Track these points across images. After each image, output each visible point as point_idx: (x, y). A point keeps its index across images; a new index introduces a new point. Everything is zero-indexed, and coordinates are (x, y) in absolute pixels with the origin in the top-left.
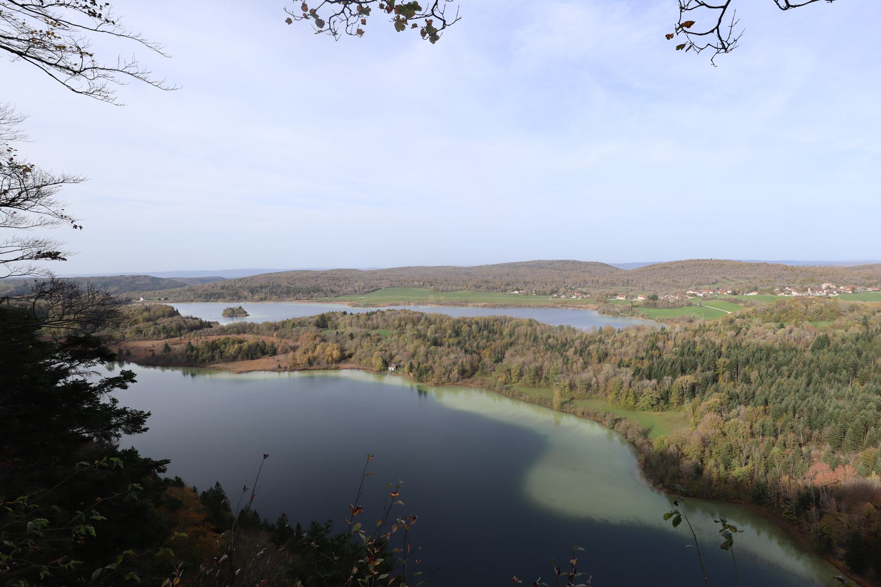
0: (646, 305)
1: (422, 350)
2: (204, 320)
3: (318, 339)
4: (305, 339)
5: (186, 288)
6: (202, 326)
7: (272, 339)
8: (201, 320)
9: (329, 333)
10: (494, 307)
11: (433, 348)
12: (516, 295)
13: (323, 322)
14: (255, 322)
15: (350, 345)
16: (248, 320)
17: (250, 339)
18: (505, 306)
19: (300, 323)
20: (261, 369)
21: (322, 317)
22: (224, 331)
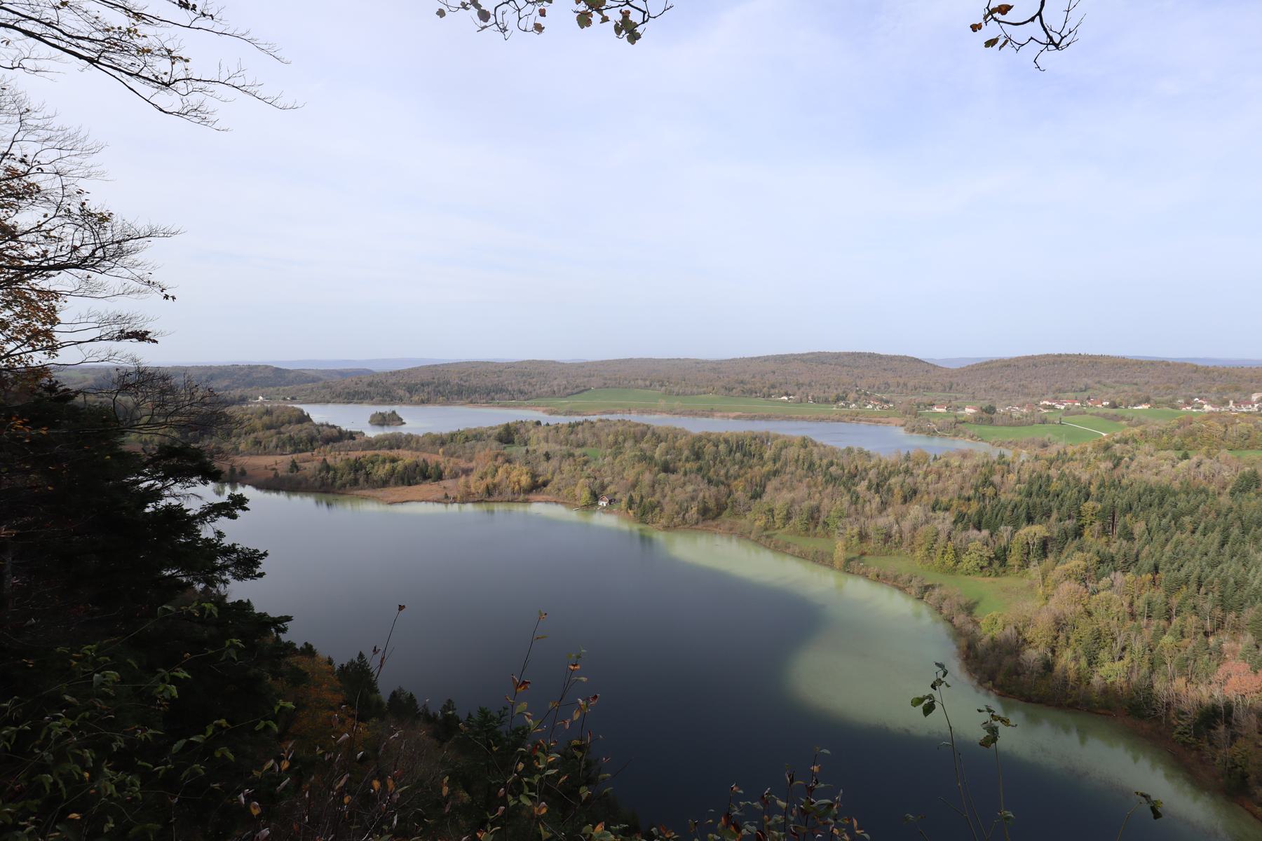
0: (978, 420)
2: (344, 428)
4: (482, 459)
5: (321, 384)
6: (338, 437)
7: (435, 458)
8: (340, 429)
9: (516, 451)
11: (662, 475)
12: (784, 401)
13: (508, 436)
14: (413, 433)
15: (545, 468)
16: (404, 430)
17: (407, 457)
18: (767, 418)
19: (475, 436)
20: (421, 498)
22: (371, 444)
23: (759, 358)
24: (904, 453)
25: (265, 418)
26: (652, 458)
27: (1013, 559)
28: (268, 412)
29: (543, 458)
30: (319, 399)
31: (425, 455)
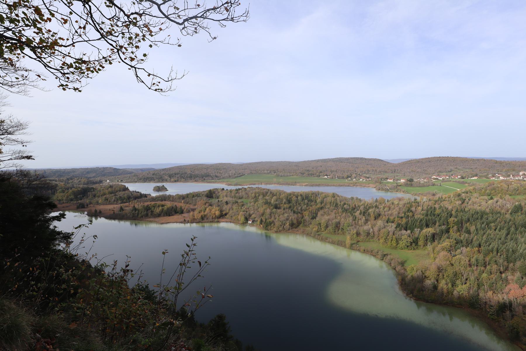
0: (406, 185)
1: (268, 211)
2: (142, 193)
5: (133, 174)
6: (140, 196)
7: (181, 204)
9: (214, 201)
10: (312, 186)
11: (274, 210)
12: (325, 178)
13: (210, 194)
15: (226, 208)
18: (319, 185)
19: (196, 195)
23: (315, 160)
24: (375, 199)
26: (270, 203)
27: (421, 243)
28: (111, 187)
29: (225, 204)
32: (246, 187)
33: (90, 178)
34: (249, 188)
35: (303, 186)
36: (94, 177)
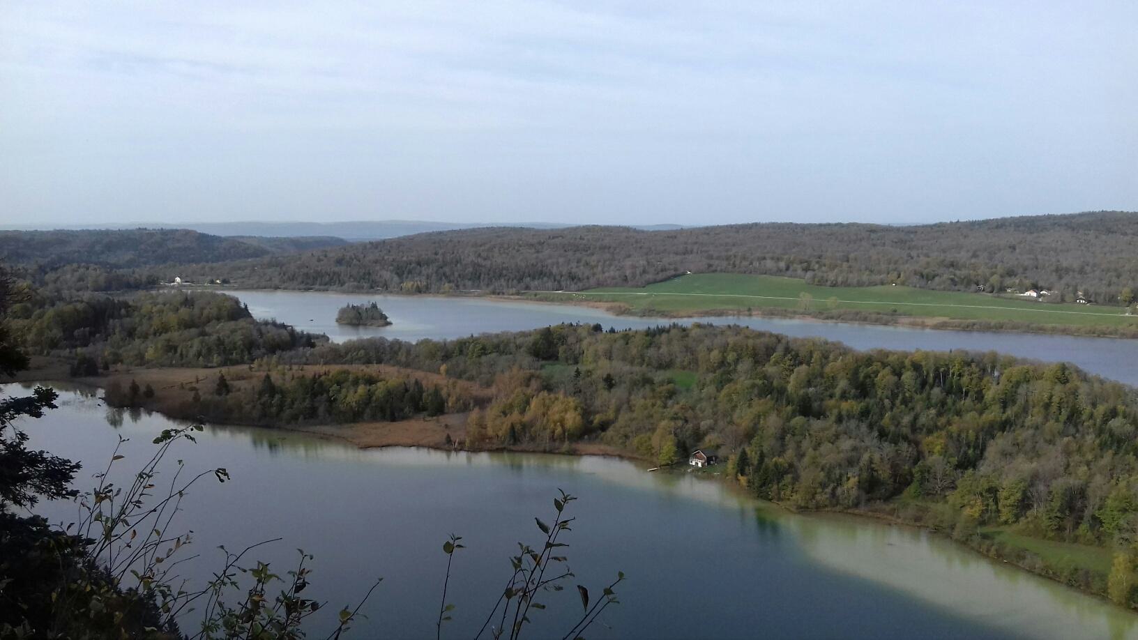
1: (773, 422)
2: (298, 329)
3: (534, 384)
5: (266, 259)
7: (436, 379)
9: (560, 371)
10: (968, 328)
11: (798, 420)
15: (606, 401)
17: (391, 376)
18: (998, 328)
21: (547, 333)
22: (338, 354)
25: (184, 311)
30: (263, 283)
31: (419, 374)
32: (686, 322)
33: (118, 267)
34: (699, 326)
35: (928, 330)
36: (130, 264)
